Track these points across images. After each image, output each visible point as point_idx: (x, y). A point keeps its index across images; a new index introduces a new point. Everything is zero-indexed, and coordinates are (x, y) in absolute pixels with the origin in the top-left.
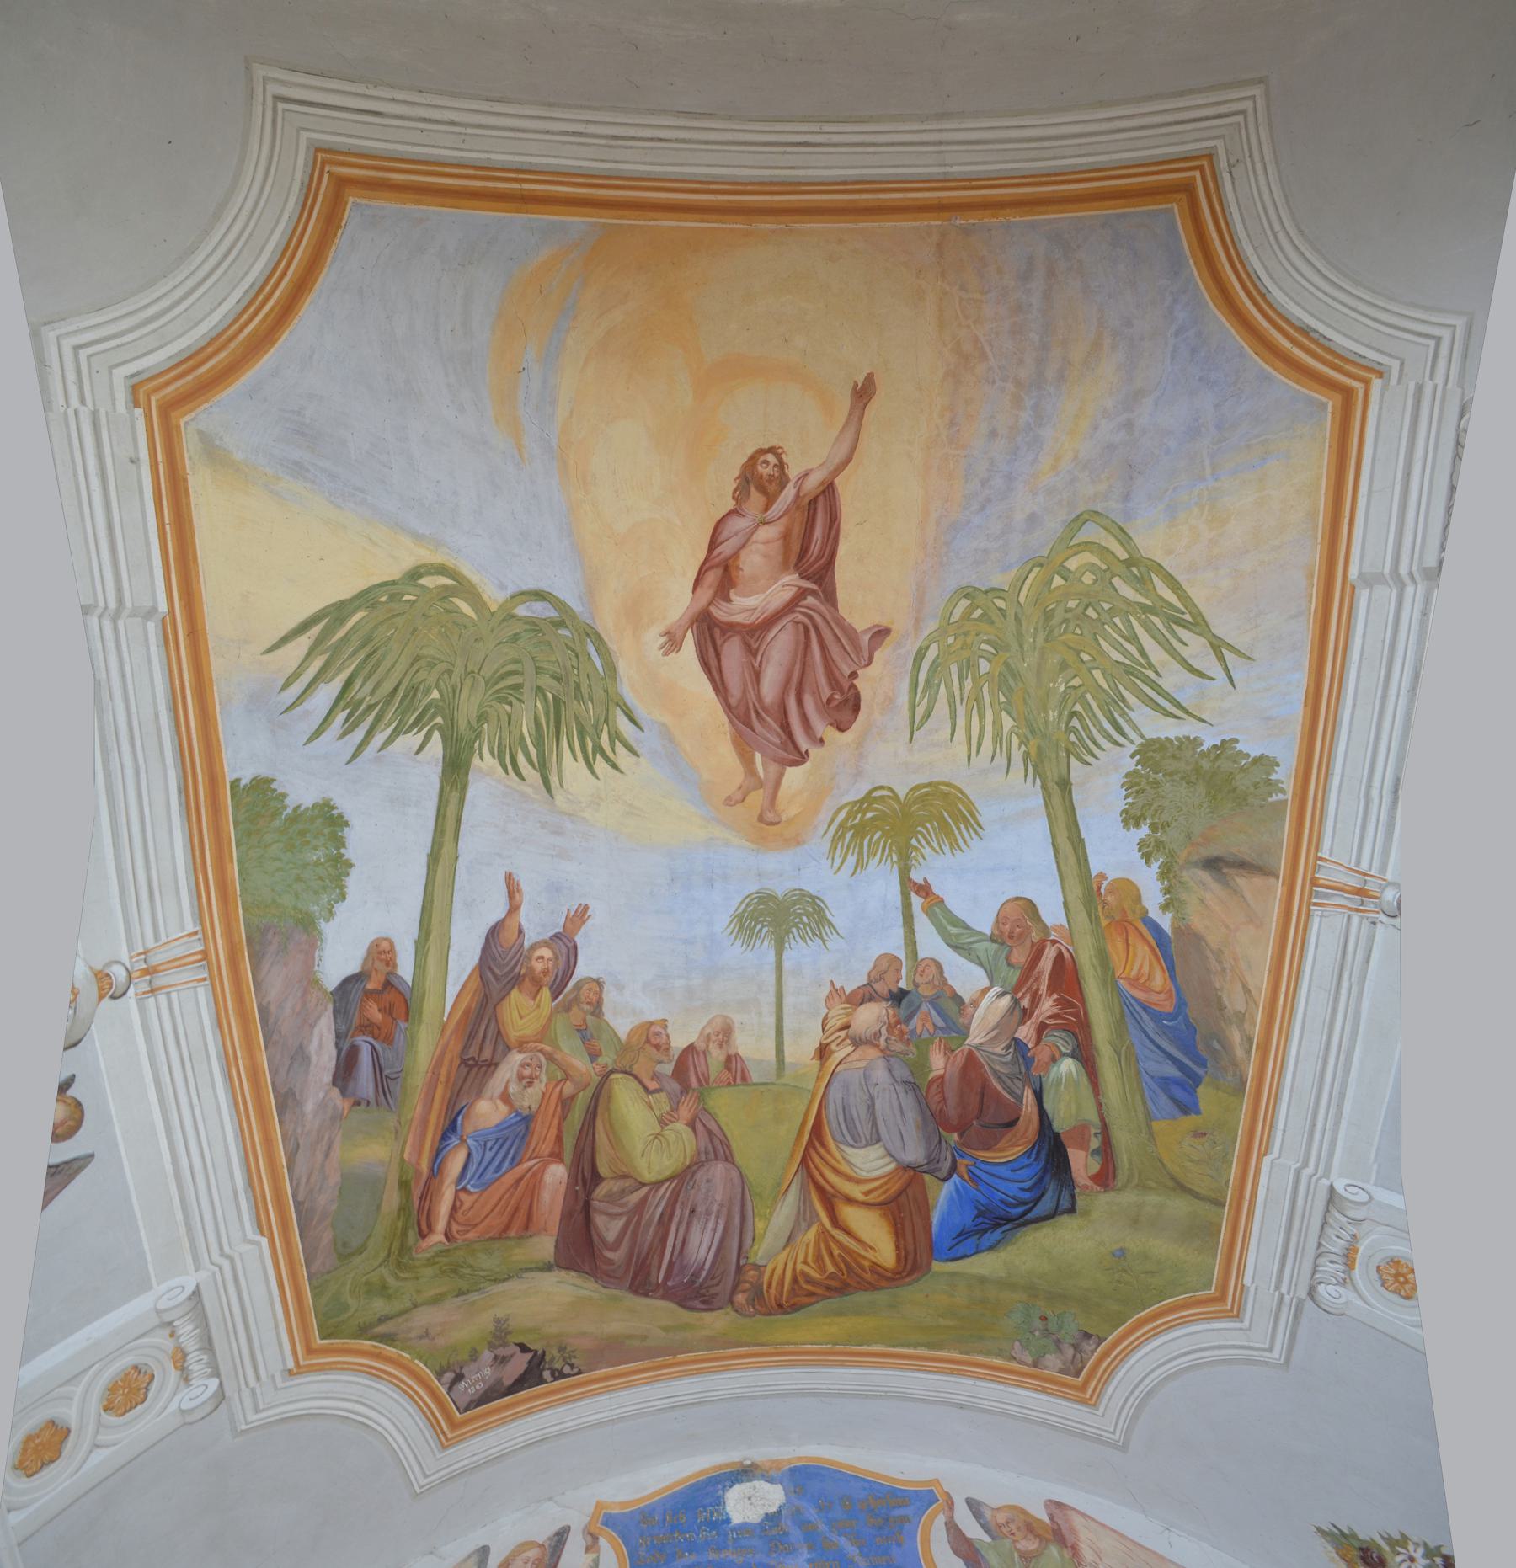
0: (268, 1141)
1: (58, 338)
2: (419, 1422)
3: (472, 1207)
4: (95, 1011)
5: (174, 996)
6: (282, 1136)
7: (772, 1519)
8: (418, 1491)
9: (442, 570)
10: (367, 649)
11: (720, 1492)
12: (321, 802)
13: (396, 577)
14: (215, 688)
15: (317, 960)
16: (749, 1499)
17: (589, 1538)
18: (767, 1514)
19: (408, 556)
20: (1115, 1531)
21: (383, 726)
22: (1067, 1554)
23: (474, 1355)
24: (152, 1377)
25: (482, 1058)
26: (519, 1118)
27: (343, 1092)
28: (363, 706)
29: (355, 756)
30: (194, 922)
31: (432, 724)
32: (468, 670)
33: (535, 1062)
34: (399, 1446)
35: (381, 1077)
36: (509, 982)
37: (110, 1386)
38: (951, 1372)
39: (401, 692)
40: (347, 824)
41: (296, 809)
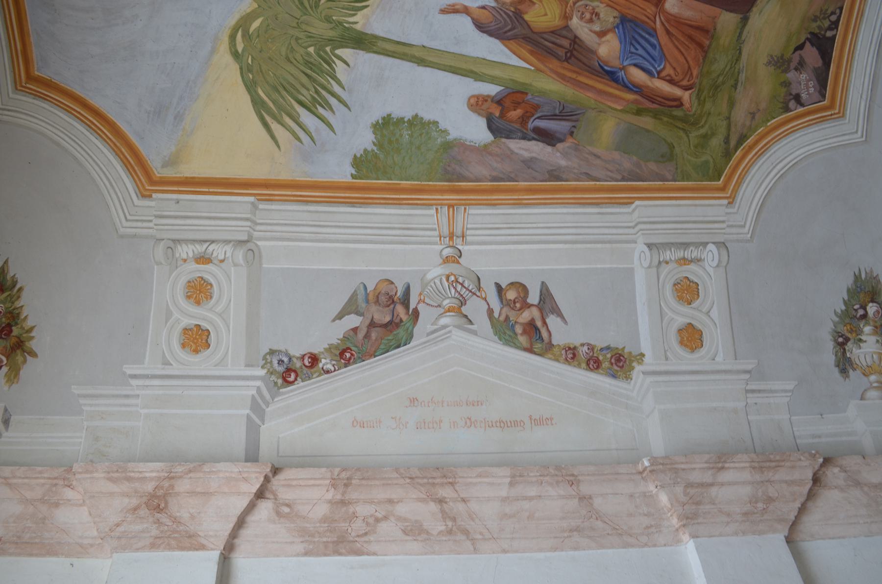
0: (575, 190)
1: (123, 227)
3: (674, 69)
4: (464, 267)
5: (469, 226)
6: (575, 181)
9: (232, 38)
10: (281, 89)
12: (372, 129)
13: (238, 67)
14: (298, 179)
15: (472, 144)
19: (224, 57)
21: (329, 85)
23: (787, 84)
24: (687, 278)
25: (568, 46)
26: (621, 27)
27: (561, 141)
28: (316, 96)
29: (346, 105)
30: (430, 209)
31: (330, 53)
32: (296, 26)
33: (581, 9)
34: (823, 146)
35: (559, 116)
36: (518, 21)
37: (678, 299)
39: (309, 72)
40: (389, 115)
41: (374, 144)
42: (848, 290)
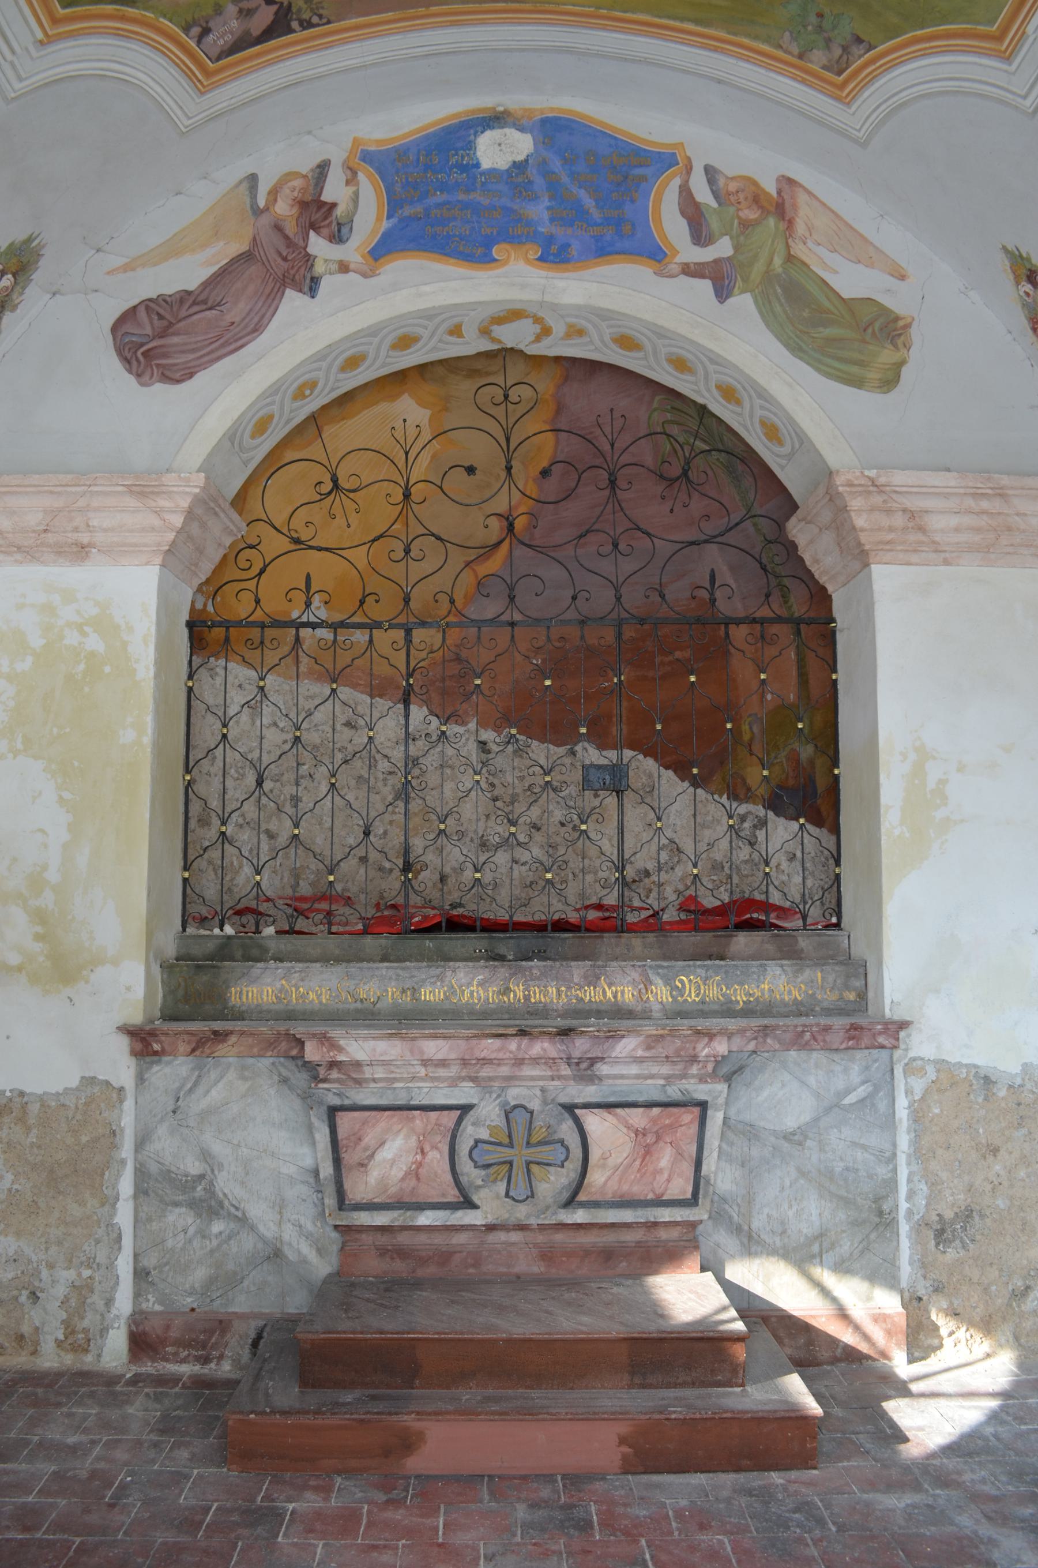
2: (173, 72)
7: (519, 167)
8: (184, 130)
11: (472, 137)
16: (500, 145)
17: (349, 172)
18: (514, 162)
20: (833, 212)
22: (782, 226)
38: (715, 49)
42: (12, 244)
